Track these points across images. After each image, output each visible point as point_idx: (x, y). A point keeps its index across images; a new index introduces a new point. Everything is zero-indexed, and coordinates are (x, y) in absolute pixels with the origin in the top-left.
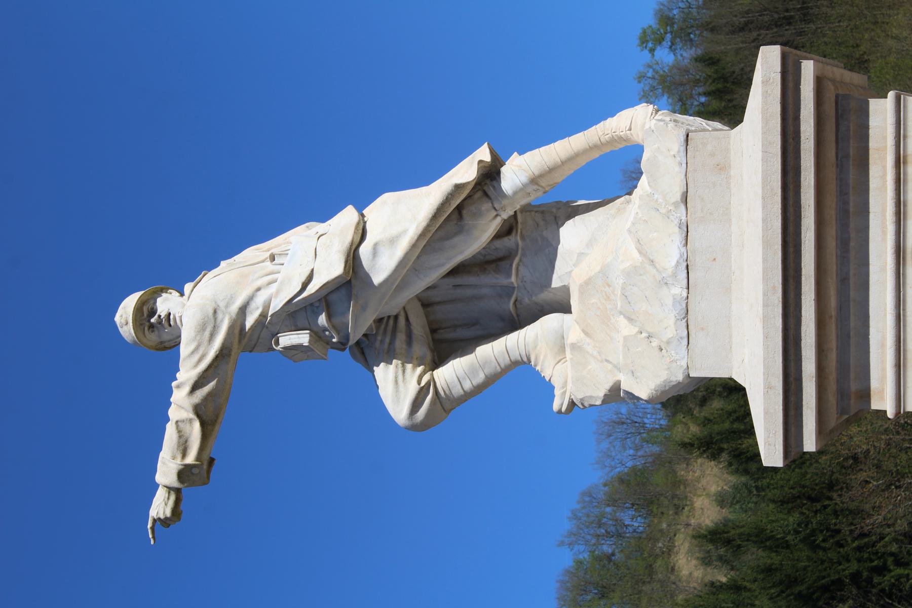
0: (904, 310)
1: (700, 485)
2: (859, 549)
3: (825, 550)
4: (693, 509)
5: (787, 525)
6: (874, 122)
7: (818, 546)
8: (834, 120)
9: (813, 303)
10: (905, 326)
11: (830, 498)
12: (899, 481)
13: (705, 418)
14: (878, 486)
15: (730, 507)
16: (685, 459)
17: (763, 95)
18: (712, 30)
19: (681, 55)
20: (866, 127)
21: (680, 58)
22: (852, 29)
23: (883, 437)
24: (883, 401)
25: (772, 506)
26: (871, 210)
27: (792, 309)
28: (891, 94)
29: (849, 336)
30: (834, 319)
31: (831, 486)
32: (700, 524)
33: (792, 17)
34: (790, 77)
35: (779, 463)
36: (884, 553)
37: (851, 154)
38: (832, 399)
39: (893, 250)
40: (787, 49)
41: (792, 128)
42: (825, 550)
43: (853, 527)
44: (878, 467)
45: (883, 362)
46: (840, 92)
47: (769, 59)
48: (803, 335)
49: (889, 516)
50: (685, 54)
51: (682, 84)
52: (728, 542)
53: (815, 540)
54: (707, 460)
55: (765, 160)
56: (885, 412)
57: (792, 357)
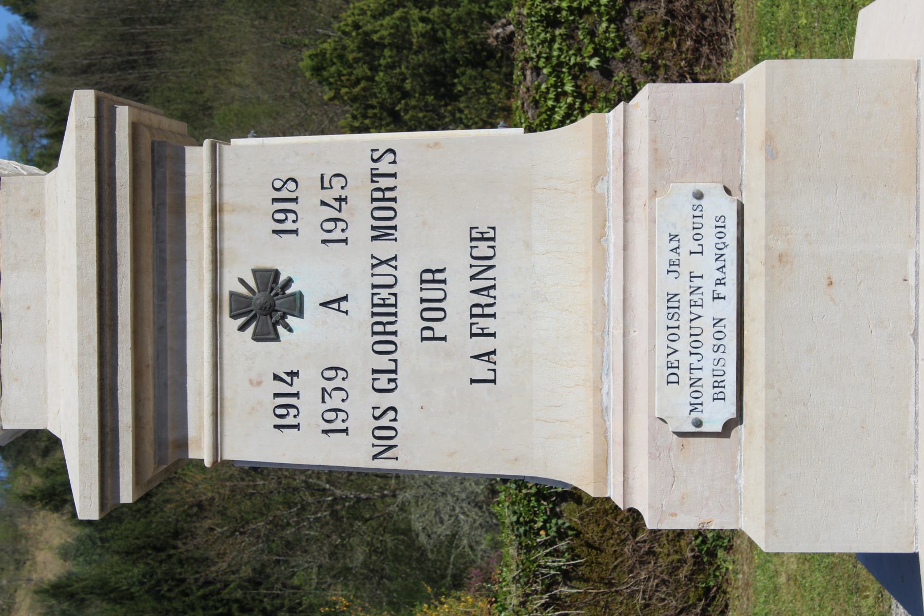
0: (221, 358)
1: (42, 539)
2: (205, 597)
3: (170, 600)
4: (34, 563)
5: (132, 577)
6: (190, 170)
7: (163, 597)
8: (150, 167)
9: (129, 352)
10: (221, 374)
11: (175, 547)
12: (243, 527)
13: (48, 469)
14: (222, 533)
15: (74, 559)
16: (27, 512)
17: (77, 140)
18: (54, 71)
19: (22, 96)
20: (183, 175)
21: (20, 99)
22: (195, 75)
23: (228, 484)
24: (201, 450)
25: (116, 558)
26: (188, 258)
27: (108, 357)
28: (207, 142)
29: (166, 384)
30: (151, 369)
31: (176, 535)
32: (42, 579)
33: (135, 61)
34: (105, 123)
35: (94, 515)
36: (228, 600)
37: (168, 201)
38: (149, 450)
39: (210, 299)
40: (102, 93)
41: (107, 174)
42: (170, 600)
43: (198, 576)
44: (222, 513)
45: (201, 410)
46: (157, 139)
47: (82, 104)
48: (119, 384)
49: (234, 562)
50: (25, 95)
51: (22, 126)
52: (72, 596)
53: (160, 591)
54: (50, 513)
55: (79, 206)
56: (203, 460)
57: (108, 408)
